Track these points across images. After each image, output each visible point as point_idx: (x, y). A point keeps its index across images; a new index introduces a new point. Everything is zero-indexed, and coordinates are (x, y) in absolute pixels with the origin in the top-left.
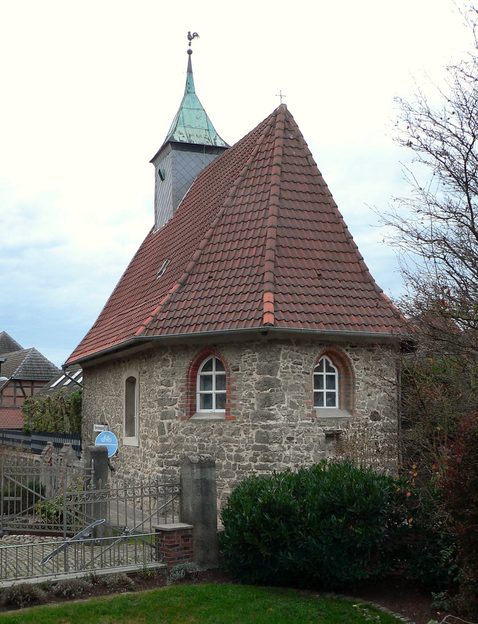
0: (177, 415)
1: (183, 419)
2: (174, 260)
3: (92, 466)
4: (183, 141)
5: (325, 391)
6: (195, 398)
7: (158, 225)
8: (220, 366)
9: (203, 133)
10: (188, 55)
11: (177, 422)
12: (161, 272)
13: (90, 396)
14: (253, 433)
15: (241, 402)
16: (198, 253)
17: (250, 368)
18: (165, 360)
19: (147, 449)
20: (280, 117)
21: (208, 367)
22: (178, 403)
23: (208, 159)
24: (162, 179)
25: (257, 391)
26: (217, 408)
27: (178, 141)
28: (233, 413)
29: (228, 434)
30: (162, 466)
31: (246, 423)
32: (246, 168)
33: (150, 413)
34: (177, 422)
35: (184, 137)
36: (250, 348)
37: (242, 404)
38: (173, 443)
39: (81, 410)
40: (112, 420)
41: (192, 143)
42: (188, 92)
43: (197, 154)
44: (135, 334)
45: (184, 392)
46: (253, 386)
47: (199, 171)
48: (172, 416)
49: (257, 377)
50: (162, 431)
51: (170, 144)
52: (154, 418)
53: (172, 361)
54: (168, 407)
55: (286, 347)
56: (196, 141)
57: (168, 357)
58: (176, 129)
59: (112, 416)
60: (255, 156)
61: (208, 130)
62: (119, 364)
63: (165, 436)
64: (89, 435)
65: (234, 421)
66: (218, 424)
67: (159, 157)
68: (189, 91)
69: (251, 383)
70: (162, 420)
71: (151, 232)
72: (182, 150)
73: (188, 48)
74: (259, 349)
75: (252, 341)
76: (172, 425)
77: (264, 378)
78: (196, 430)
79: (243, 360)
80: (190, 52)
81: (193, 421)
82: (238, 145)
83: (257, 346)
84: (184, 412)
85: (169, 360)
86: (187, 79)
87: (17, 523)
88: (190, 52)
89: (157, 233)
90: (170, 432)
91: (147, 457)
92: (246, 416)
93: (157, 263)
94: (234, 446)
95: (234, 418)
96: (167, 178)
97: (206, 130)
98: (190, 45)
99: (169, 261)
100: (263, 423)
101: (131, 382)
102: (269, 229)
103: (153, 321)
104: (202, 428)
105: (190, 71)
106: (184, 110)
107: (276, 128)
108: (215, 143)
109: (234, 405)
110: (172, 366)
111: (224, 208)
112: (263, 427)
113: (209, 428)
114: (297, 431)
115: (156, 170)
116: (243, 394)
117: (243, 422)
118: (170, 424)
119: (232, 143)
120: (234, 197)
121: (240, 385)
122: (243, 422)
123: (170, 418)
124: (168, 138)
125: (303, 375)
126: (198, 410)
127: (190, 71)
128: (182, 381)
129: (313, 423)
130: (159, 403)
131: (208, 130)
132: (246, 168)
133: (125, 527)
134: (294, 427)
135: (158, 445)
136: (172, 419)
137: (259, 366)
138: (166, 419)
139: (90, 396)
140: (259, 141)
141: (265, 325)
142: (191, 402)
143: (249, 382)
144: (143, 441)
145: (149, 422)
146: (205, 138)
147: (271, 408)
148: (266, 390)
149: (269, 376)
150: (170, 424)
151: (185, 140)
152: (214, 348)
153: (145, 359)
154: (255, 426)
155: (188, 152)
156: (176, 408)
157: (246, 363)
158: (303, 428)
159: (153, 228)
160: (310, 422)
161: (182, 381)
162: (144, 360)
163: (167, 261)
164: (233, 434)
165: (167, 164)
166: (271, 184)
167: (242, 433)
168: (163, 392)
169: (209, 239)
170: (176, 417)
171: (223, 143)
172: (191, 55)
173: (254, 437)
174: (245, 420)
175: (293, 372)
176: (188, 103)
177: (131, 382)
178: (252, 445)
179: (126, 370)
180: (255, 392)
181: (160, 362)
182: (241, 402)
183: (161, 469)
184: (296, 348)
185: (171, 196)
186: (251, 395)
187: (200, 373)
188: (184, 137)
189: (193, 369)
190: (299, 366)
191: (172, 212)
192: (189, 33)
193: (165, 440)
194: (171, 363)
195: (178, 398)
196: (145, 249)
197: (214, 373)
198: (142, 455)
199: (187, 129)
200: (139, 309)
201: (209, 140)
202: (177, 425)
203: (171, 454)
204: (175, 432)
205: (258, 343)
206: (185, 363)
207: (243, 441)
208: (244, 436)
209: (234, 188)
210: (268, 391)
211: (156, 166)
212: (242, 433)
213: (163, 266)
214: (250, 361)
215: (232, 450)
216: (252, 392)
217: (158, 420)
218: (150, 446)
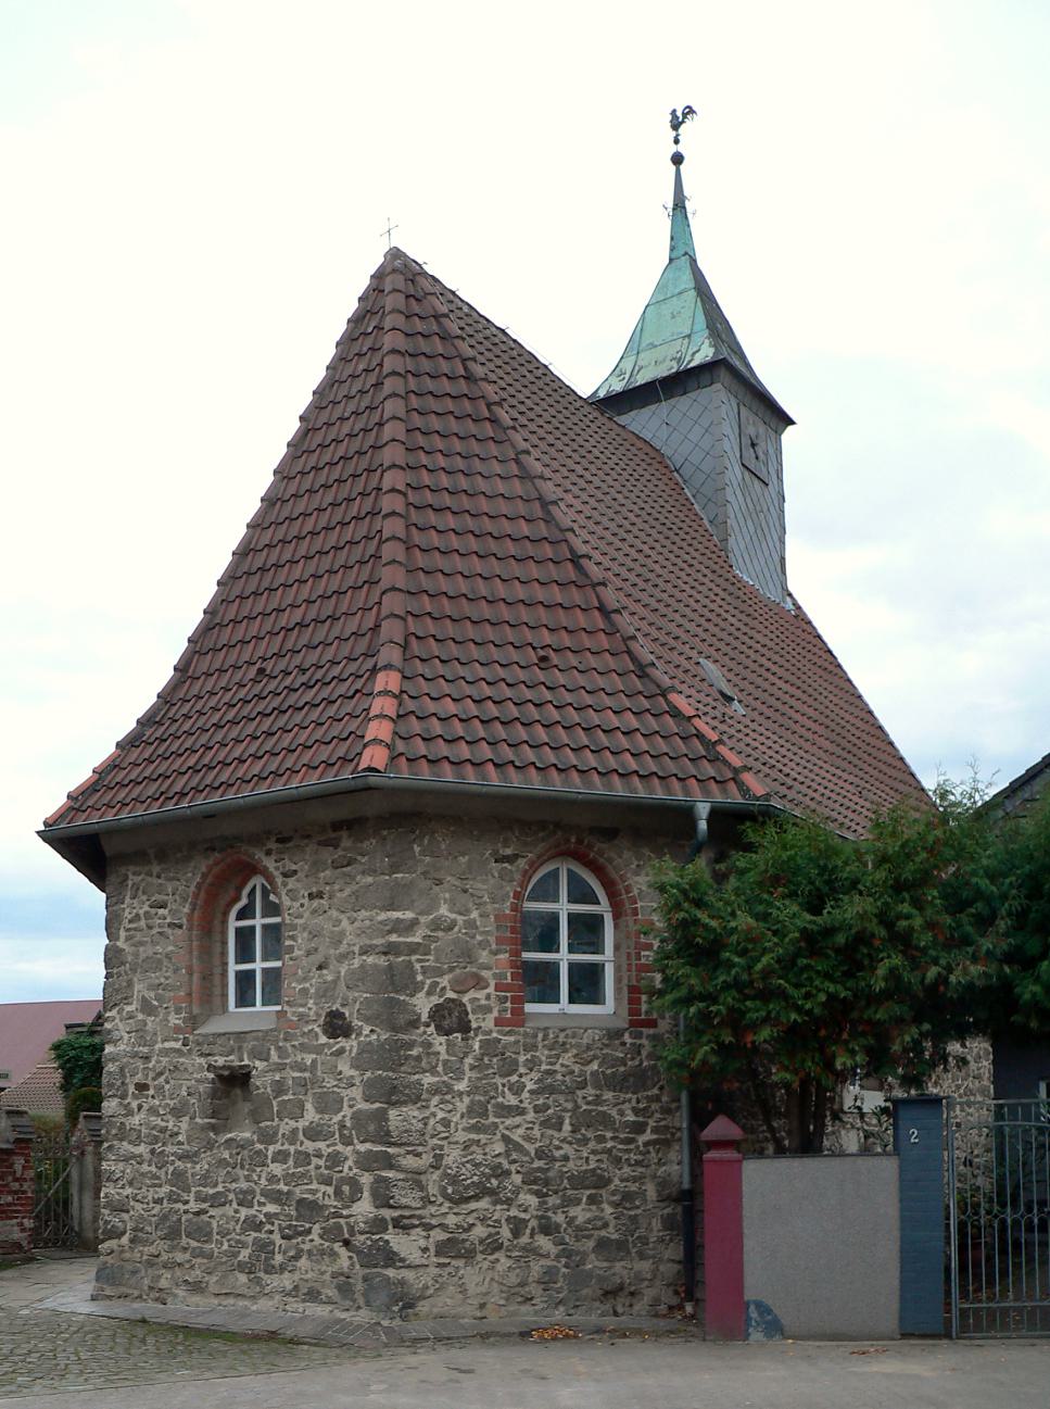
5: (258, 966)
8: (272, 909)
10: (674, 167)
55: (138, 869)
73: (673, 149)
80: (677, 159)
88: (677, 159)
98: (676, 141)
105: (679, 205)
114: (153, 1069)
125: (169, 931)
127: (679, 205)
129: (185, 1049)
134: (147, 1058)
158: (165, 1060)
160: (178, 1045)
172: (682, 167)
175: (150, 927)
184: (156, 869)
190: (161, 911)
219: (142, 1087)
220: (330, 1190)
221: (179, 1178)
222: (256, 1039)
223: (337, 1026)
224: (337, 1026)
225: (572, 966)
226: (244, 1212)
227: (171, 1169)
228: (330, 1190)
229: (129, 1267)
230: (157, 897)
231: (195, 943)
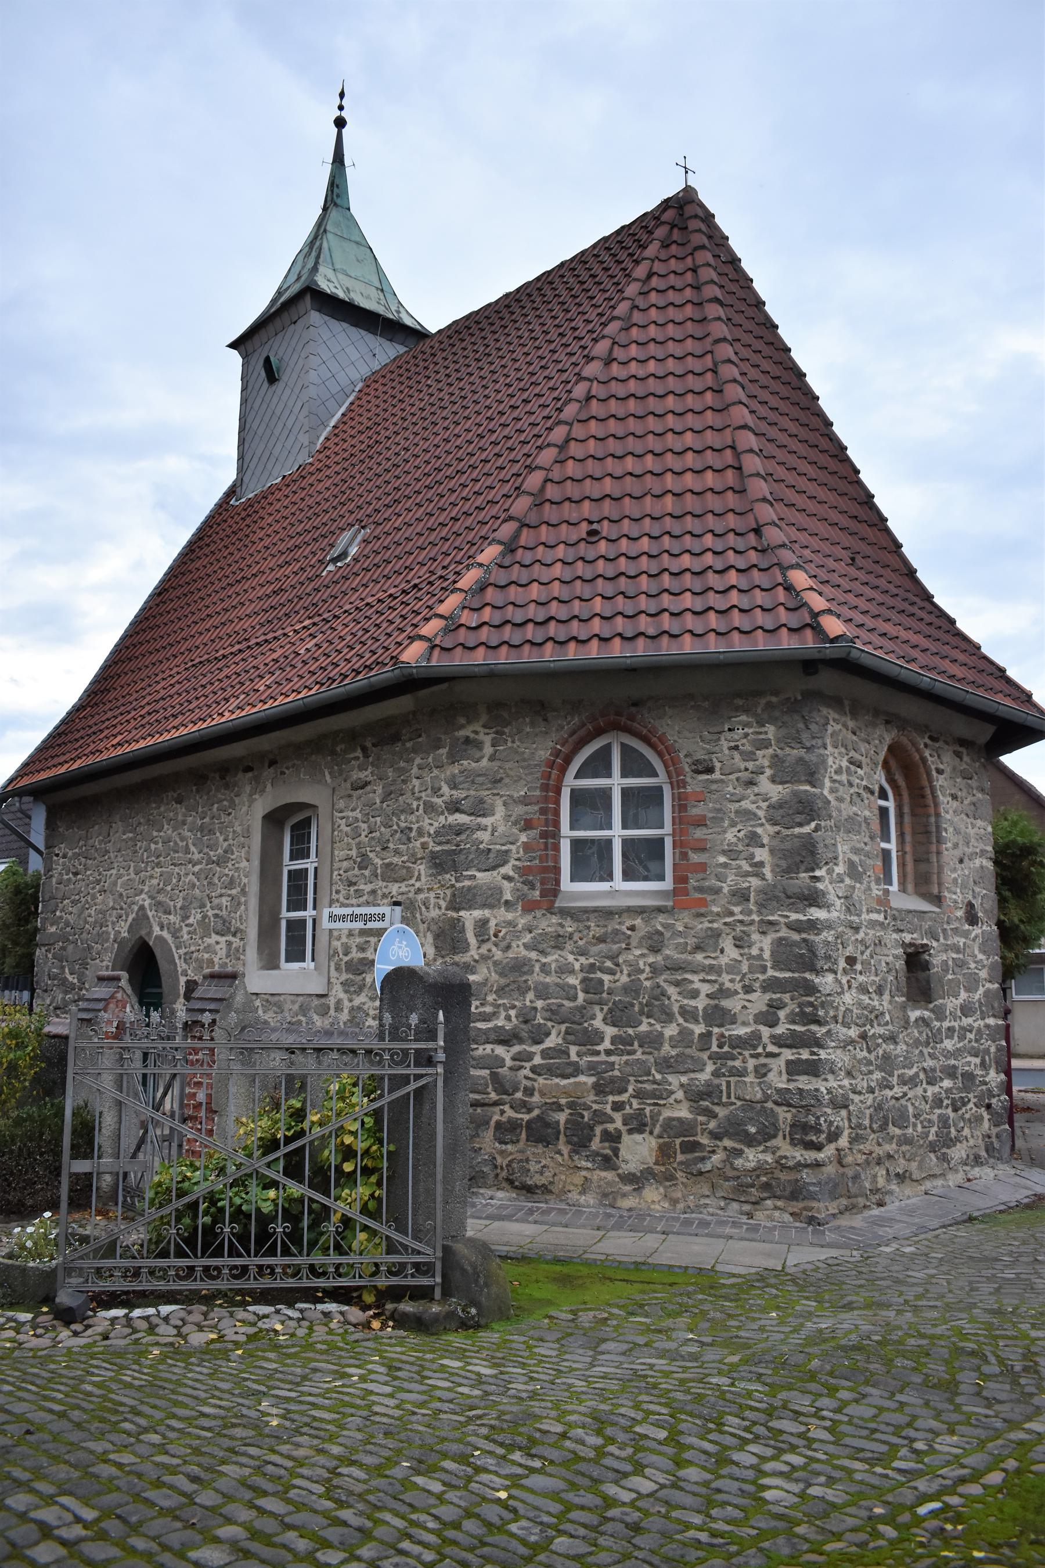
0: (508, 896)
1: (529, 907)
6: (557, 848)
8: (633, 765)
11: (510, 916)
13: (76, 874)
14: (763, 944)
15: (722, 859)
17: (750, 765)
18: (467, 741)
21: (599, 765)
22: (513, 862)
23: (386, 351)
24: (272, 377)
25: (772, 829)
26: (628, 876)
28: (700, 889)
29: (682, 948)
31: (740, 917)
34: (510, 916)
36: (746, 711)
37: (725, 865)
38: (494, 977)
39: (36, 913)
43: (363, 332)
45: (534, 833)
46: (761, 813)
47: (365, 372)
48: (491, 899)
49: (776, 792)
54: (479, 875)
57: (476, 733)
64: (70, 978)
65: (703, 910)
66: (646, 921)
69: (752, 807)
73: (338, 113)
74: (777, 713)
75: (759, 694)
77: (795, 794)
78: (576, 937)
79: (725, 745)
80: (340, 123)
83: (769, 706)
84: (533, 887)
85: (482, 743)
88: (340, 123)
92: (741, 896)
94: (703, 981)
95: (703, 903)
100: (794, 916)
103: (447, 631)
104: (596, 931)
109: (702, 867)
112: (796, 927)
113: (616, 932)
116: (730, 836)
117: (731, 914)
118: (483, 923)
119: (434, 320)
121: (719, 810)
122: (731, 914)
123: (484, 906)
126: (567, 885)
128: (525, 801)
137: (776, 761)
143: (746, 804)
147: (818, 873)
148: (801, 825)
149: (808, 788)
150: (483, 923)
151: (341, 295)
152: (633, 709)
153: (364, 749)
154: (771, 923)
155: (345, 325)
156: (508, 878)
157: (736, 753)
161: (525, 801)
162: (359, 753)
164: (698, 948)
167: (727, 943)
168: (459, 830)
169: (562, 447)
170: (507, 902)
172: (345, 131)
173: (767, 955)
174: (737, 909)
178: (761, 977)
180: (766, 832)
182: (722, 859)
186: (753, 839)
187: (570, 781)
194: (488, 750)
195: (513, 848)
202: (511, 924)
204: (503, 944)
205: (774, 699)
207: (733, 968)
208: (732, 953)
210: (806, 829)
211: (245, 357)
212: (727, 943)
214: (748, 748)
215: (695, 994)
216: (759, 830)
219: (851, 961)
220: (978, 1060)
221: (887, 1063)
222: (931, 919)
223: (972, 918)
224: (972, 918)
225: (626, 842)
226: (931, 1090)
227: (881, 1052)
228: (978, 1060)
229: (850, 1172)
230: (857, 756)
231: (933, 819)
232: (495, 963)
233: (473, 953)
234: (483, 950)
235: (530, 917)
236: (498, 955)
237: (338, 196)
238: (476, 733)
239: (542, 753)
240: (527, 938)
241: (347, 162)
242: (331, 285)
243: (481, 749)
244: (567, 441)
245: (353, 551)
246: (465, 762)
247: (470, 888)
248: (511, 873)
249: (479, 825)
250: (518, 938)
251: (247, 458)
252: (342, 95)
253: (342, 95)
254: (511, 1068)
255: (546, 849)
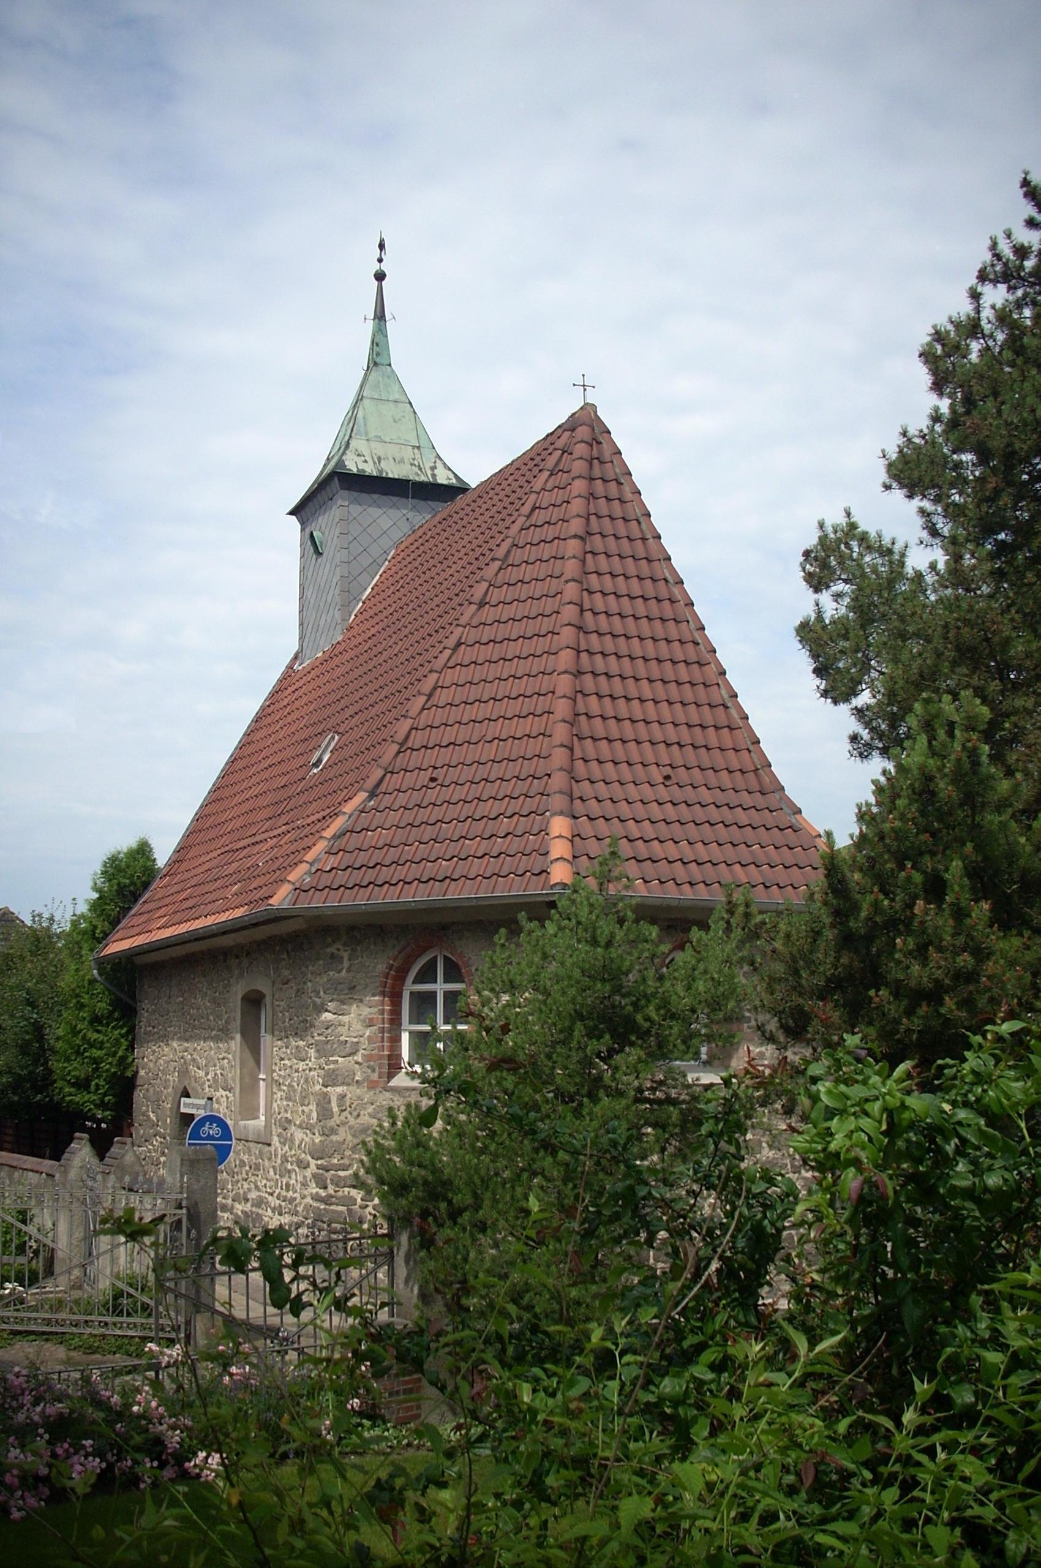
1: (372, 1085)
2: (348, 738)
3: (185, 1190)
4: (364, 471)
7: (307, 652)
8: (453, 973)
9: (408, 453)
12: (320, 760)
13: (154, 1027)
16: (405, 726)
18: (332, 956)
19: (291, 1149)
20: (583, 432)
21: (427, 974)
24: (319, 554)
27: (355, 470)
30: (325, 1188)
32: (509, 541)
33: (297, 1071)
35: (366, 461)
38: (350, 1138)
40: (207, 1083)
41: (384, 475)
42: (376, 364)
44: (271, 901)
48: (348, 1080)
50: (325, 1113)
51: (336, 479)
52: (306, 1081)
53: (349, 960)
54: (340, 1059)
56: (393, 471)
57: (339, 950)
58: (348, 444)
59: (207, 1074)
60: (528, 517)
61: (419, 448)
62: (225, 961)
63: (331, 1123)
64: (152, 1115)
67: (310, 504)
68: (378, 360)
70: (326, 1087)
71: (290, 667)
72: (361, 491)
73: (376, 266)
76: (348, 1098)
80: (380, 277)
81: (394, 1090)
82: (489, 486)
85: (342, 958)
86: (374, 335)
87: (15, 1314)
88: (380, 277)
89: (305, 672)
90: (346, 1113)
91: (289, 1167)
93: (311, 741)
96: (328, 551)
97: (414, 447)
98: (380, 260)
99: (337, 737)
101: (254, 1002)
102: (562, 676)
105: (380, 315)
106: (366, 402)
107: (574, 456)
108: (434, 476)
110: (349, 970)
111: (461, 629)
115: (303, 530)
120: (482, 604)
123: (343, 1084)
124: (333, 463)
127: (380, 315)
130: (318, 1051)
131: (419, 448)
132: (509, 541)
133: (279, 1329)
135: (317, 1141)
136: (348, 1085)
138: (334, 1085)
139: (154, 1027)
140: (538, 485)
141: (553, 887)
142: (391, 1049)
144: (280, 1130)
145: (295, 1091)
146: (412, 465)
150: (342, 1097)
151: (370, 469)
153: (288, 953)
159: (296, 657)
162: (285, 956)
163: (333, 738)
165: (327, 525)
166: (563, 579)
169: (430, 696)
170: (357, 1081)
171: (451, 476)
172: (384, 283)
176: (376, 386)
177: (254, 1002)
179: (241, 975)
181: (321, 962)
183: (323, 1193)
185: (337, 591)
187: (410, 987)
188: (366, 461)
189: (395, 978)
191: (339, 627)
192: (821, 525)
193: (333, 1131)
194: (346, 964)
196: (278, 706)
197: (440, 987)
198: (279, 1161)
199: (373, 445)
200: (271, 843)
201: (420, 469)
202: (359, 1098)
203: (346, 1161)
204: (355, 1113)
206: (379, 964)
209: (485, 585)
211: (303, 524)
213: (323, 746)
217: (318, 1087)
218: (297, 1143)
232: (350, 1128)
233: (337, 1119)
234: (342, 1118)
235: (372, 1093)
236: (352, 1121)
237: (378, 354)
238: (339, 950)
239: (380, 966)
240: (370, 1109)
241: (388, 316)
242: (360, 460)
243: (342, 963)
244: (435, 688)
245: (325, 758)
246: (331, 973)
247: (334, 1070)
248: (360, 1060)
249: (340, 1021)
250: (365, 1109)
251: (305, 626)
252: (382, 246)
253: (382, 246)
254: (360, 1207)
255: (383, 1041)
